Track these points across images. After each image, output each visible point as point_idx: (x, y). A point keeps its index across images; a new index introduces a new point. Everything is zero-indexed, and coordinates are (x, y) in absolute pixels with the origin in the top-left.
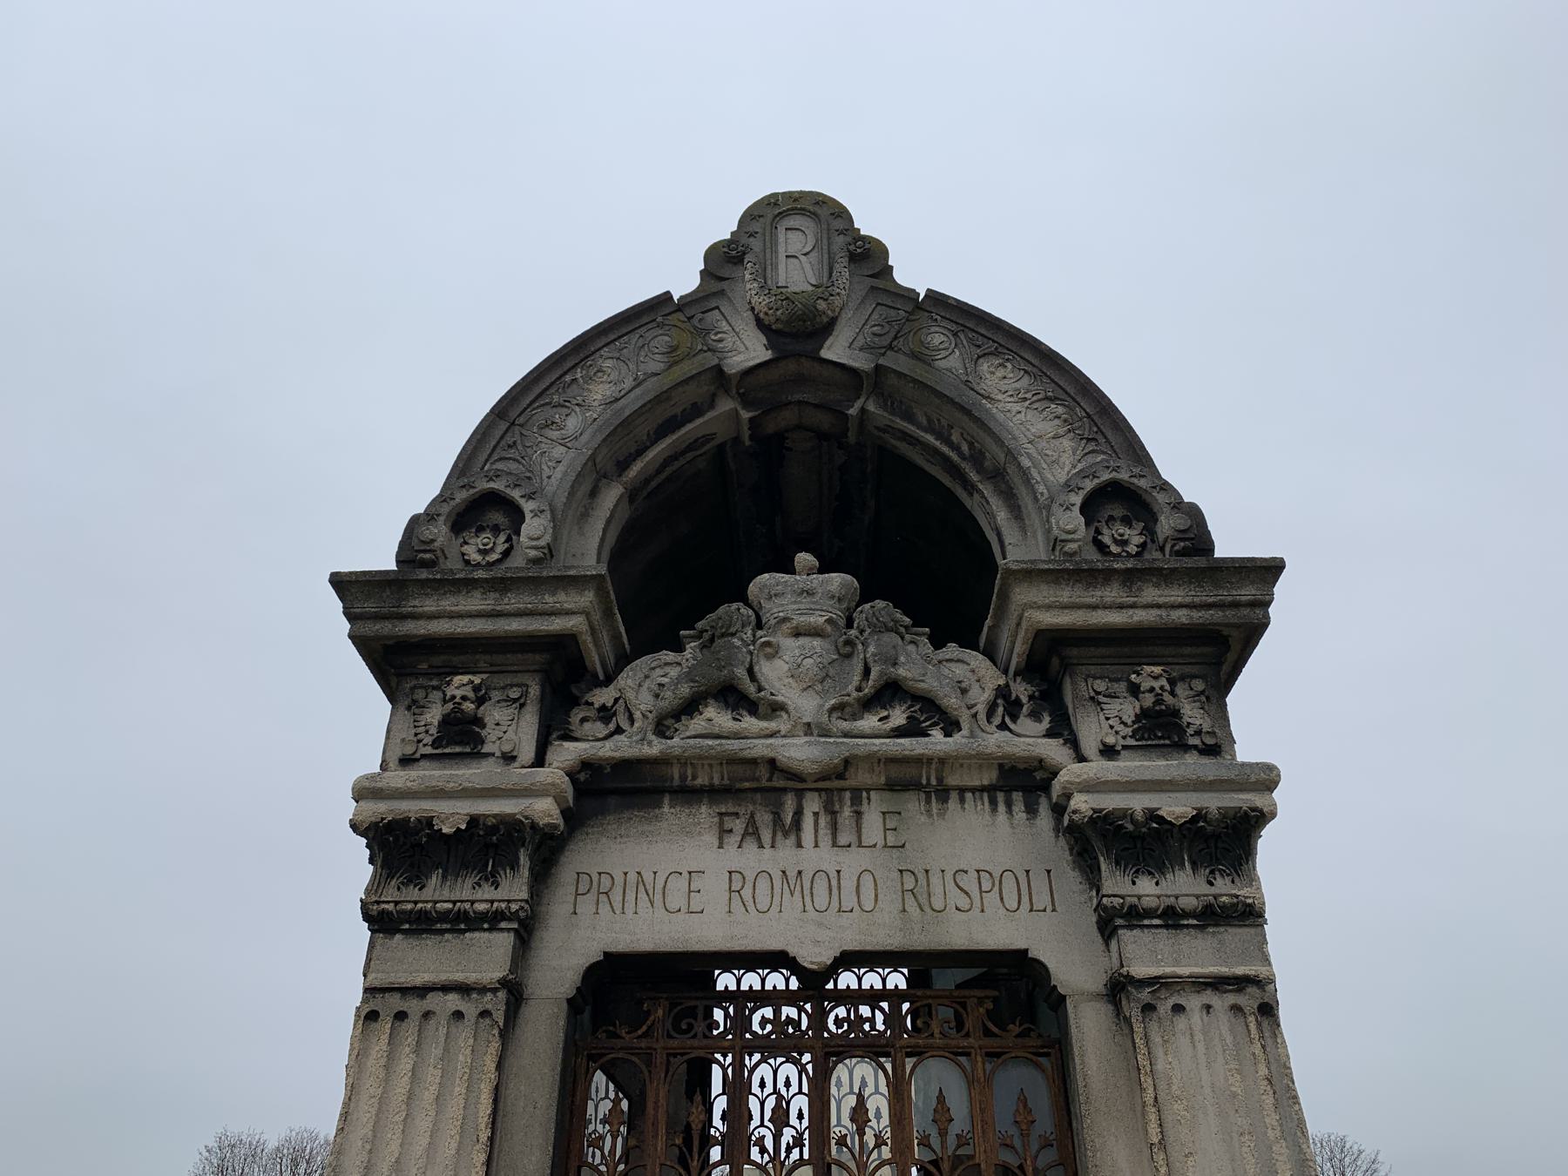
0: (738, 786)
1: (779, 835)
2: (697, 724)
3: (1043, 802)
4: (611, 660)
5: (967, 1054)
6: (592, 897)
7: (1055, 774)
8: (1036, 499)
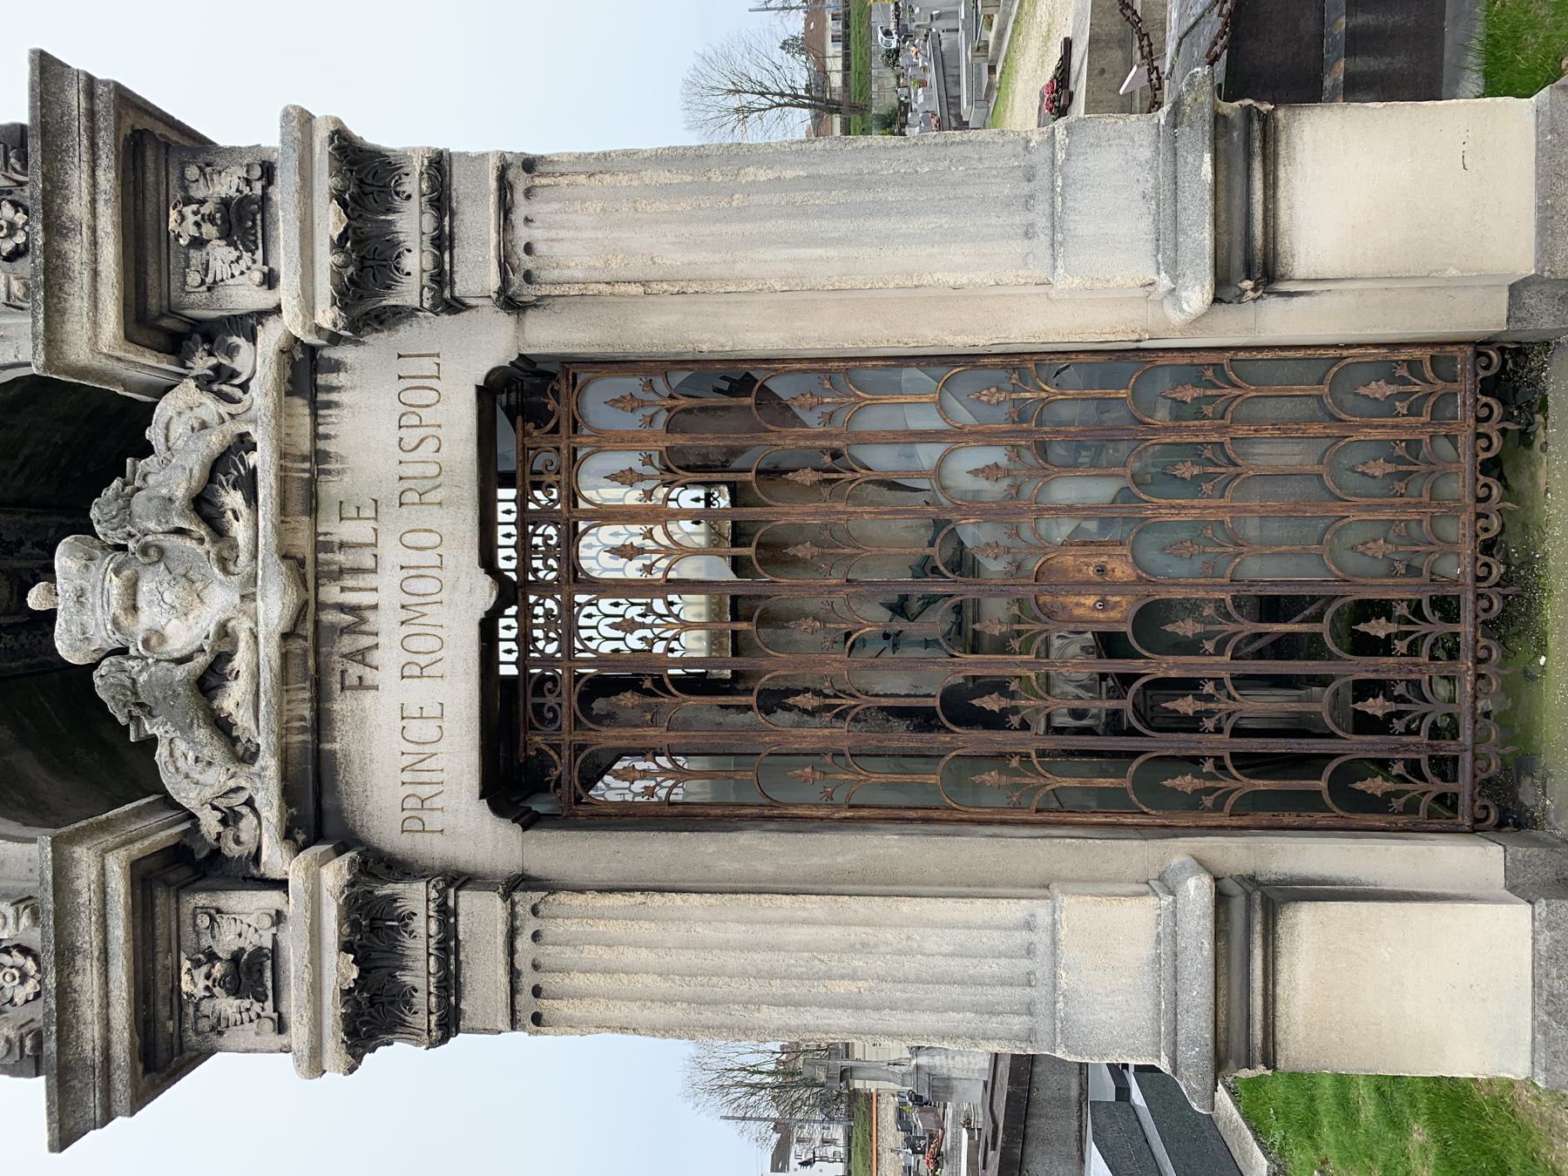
0: (312, 672)
1: (364, 628)
2: (243, 720)
3: (327, 353)
4: (170, 814)
5: (575, 450)
6: (425, 816)
7: (297, 339)
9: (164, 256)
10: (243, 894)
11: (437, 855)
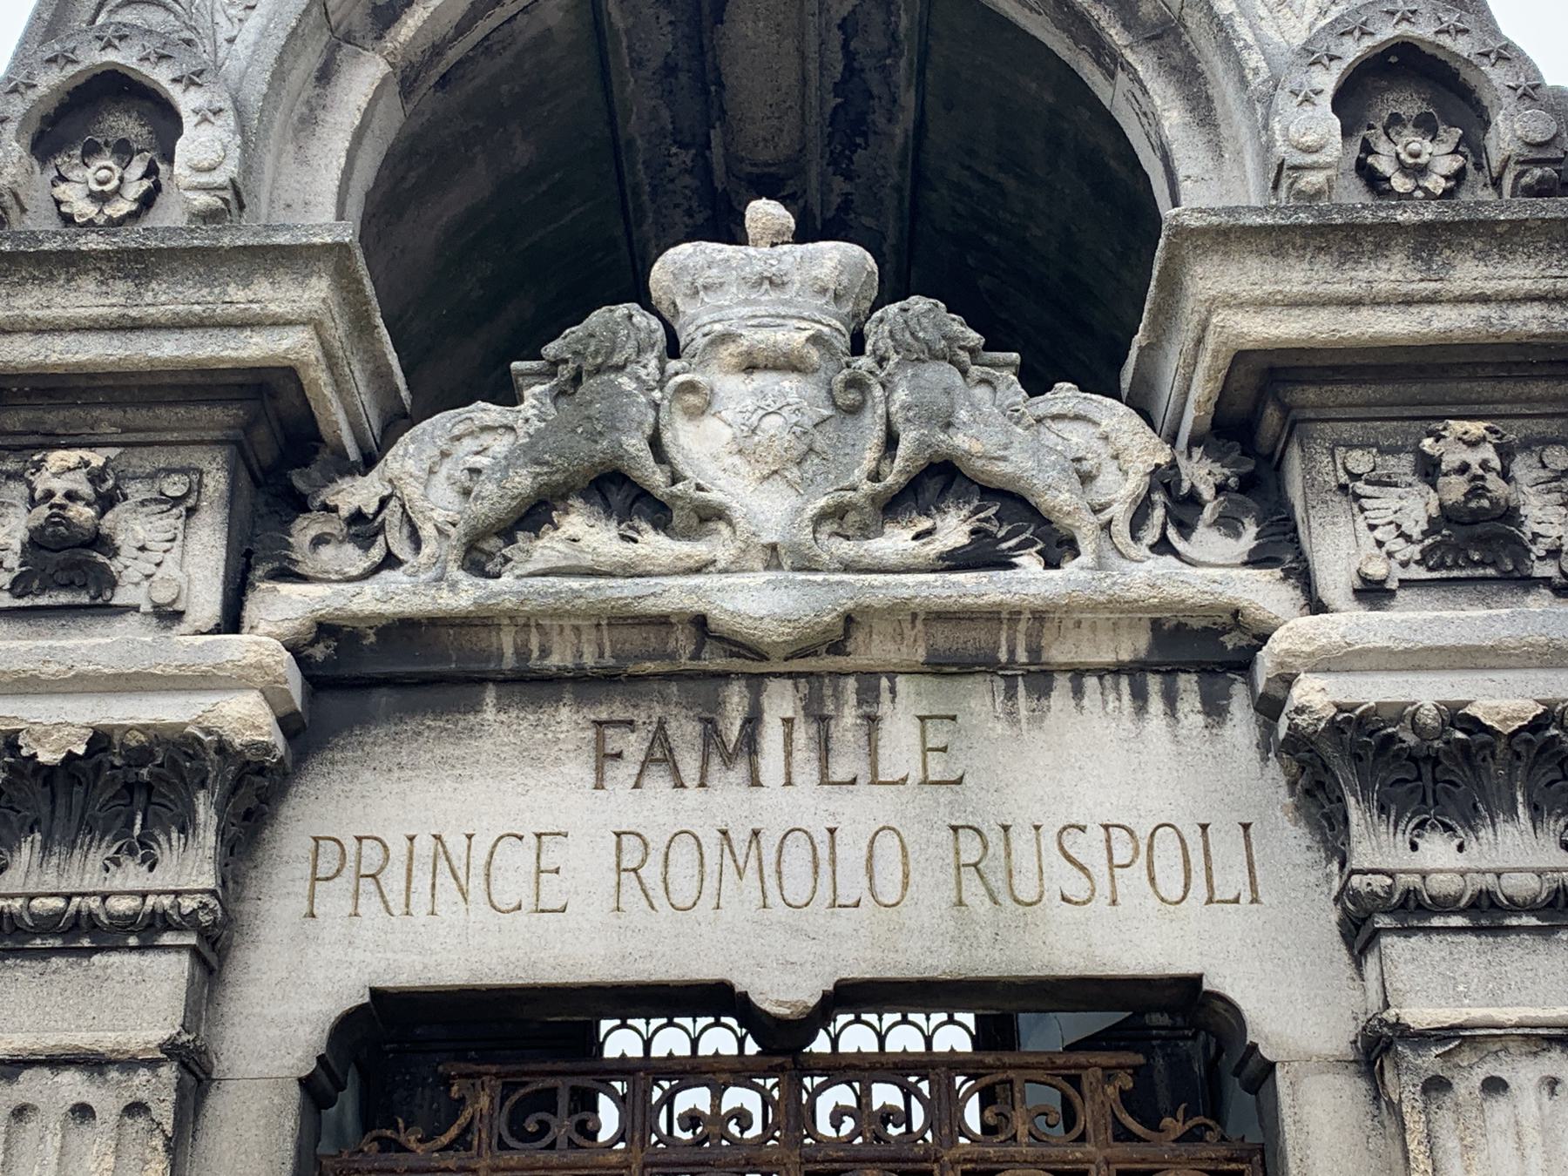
2: (548, 548)
4: (373, 423)
6: (345, 882)
7: (1264, 638)
8: (1243, 82)
9: (1396, 412)
10: (221, 553)
11: (264, 905)
